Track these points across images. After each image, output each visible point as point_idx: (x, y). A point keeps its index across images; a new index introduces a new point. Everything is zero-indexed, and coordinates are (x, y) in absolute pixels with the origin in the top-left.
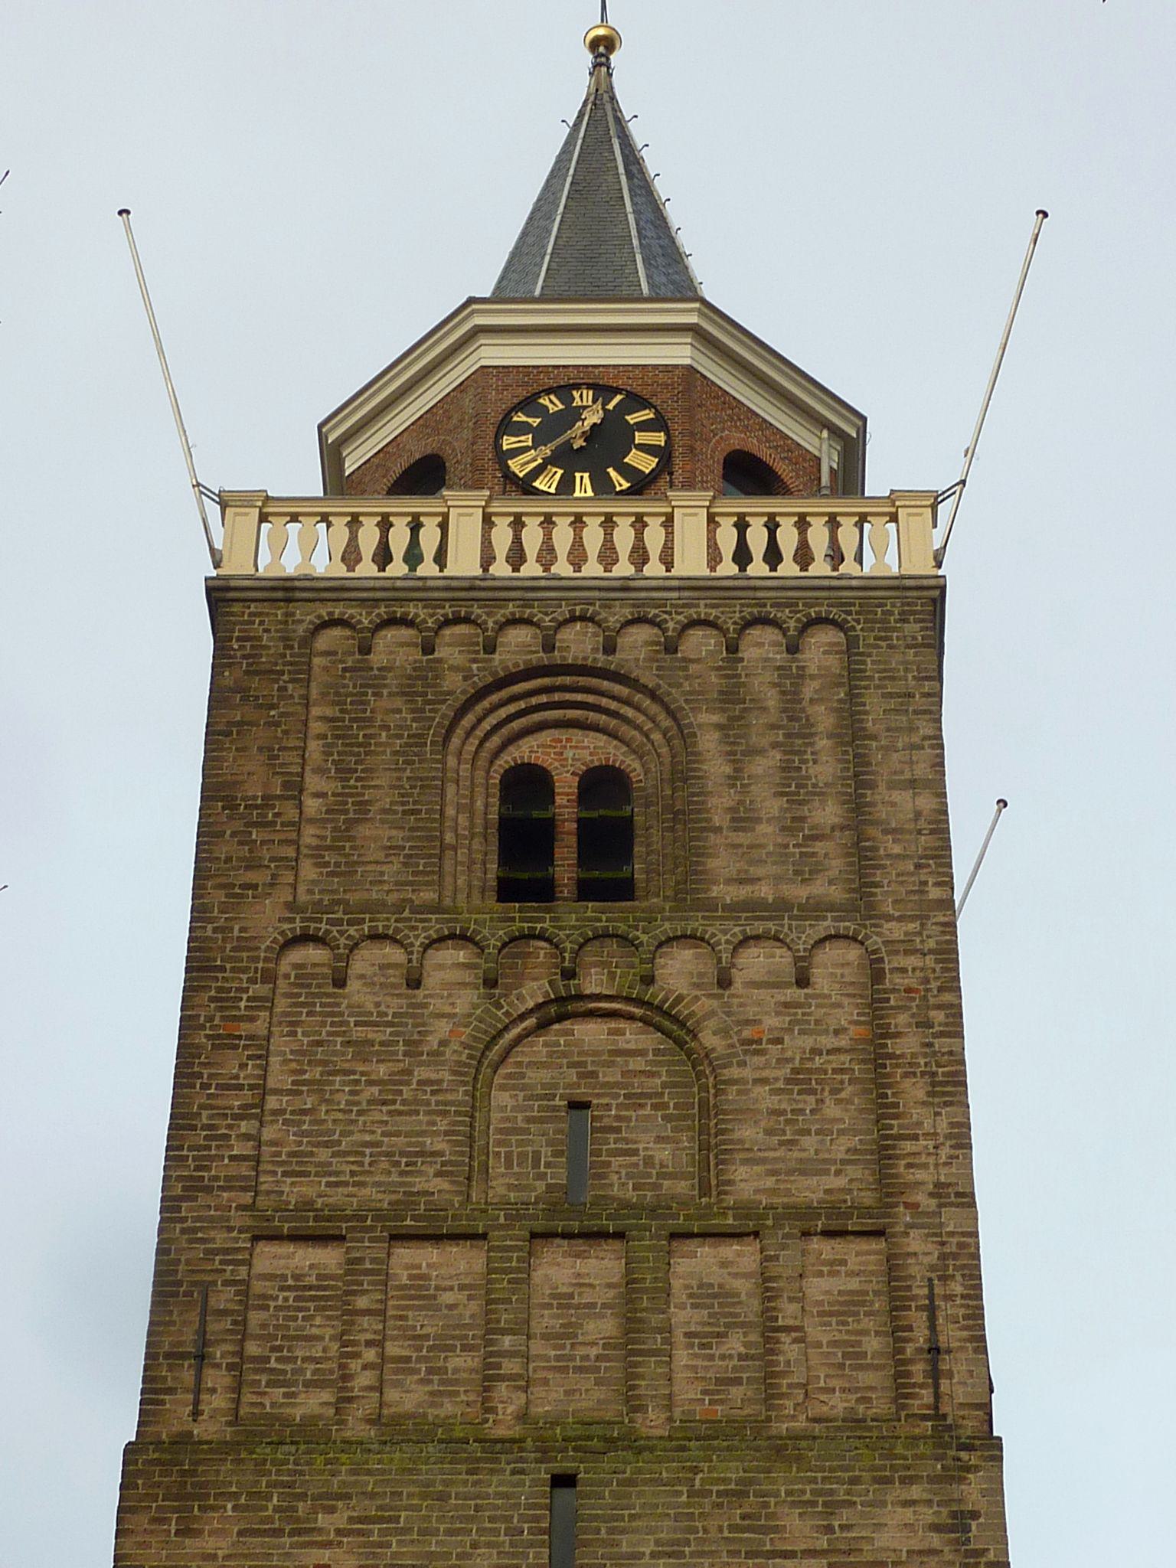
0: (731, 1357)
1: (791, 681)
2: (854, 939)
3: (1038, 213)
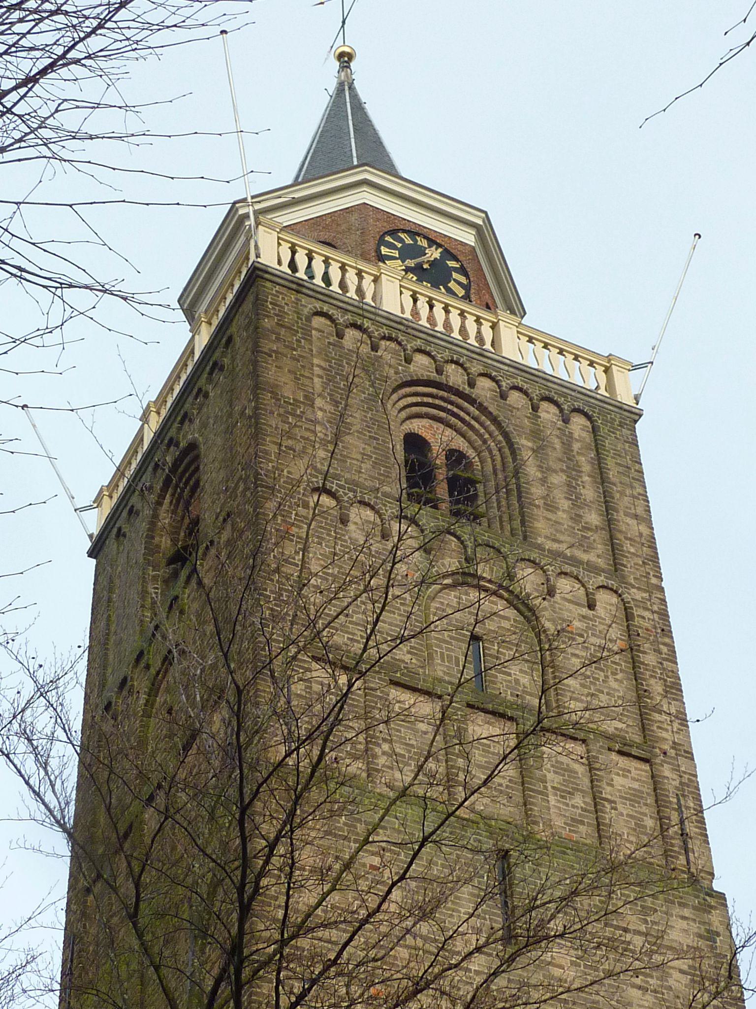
0: (577, 807)
1: (568, 441)
2: (616, 592)
3: (695, 235)
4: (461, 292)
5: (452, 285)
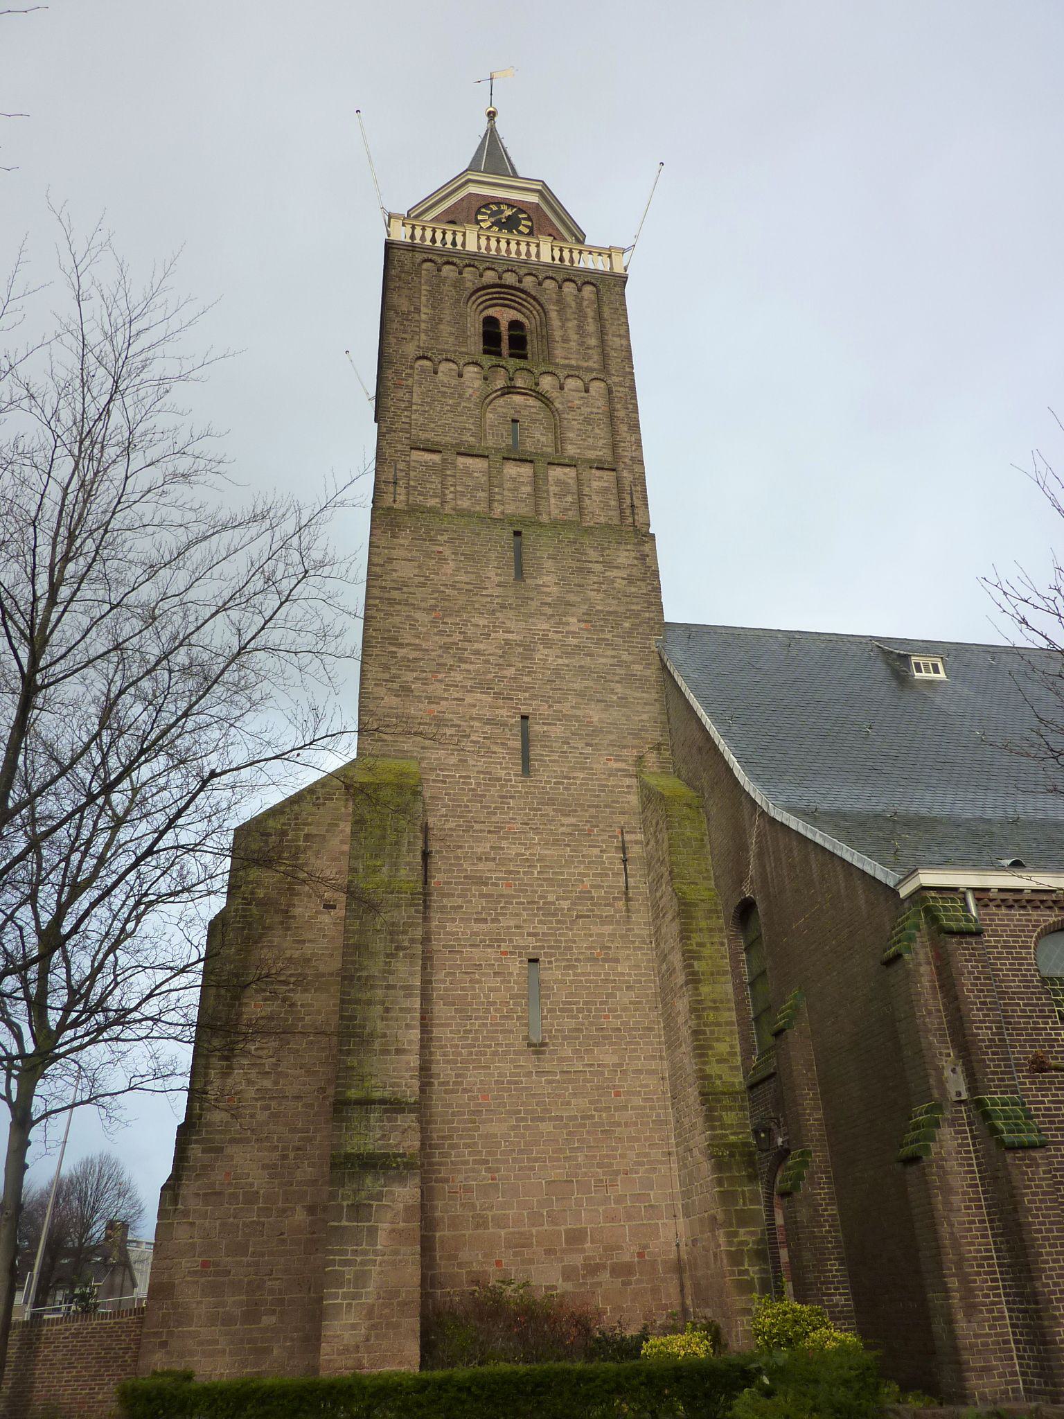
1: (579, 301)
4: (526, 231)
5: (521, 228)
